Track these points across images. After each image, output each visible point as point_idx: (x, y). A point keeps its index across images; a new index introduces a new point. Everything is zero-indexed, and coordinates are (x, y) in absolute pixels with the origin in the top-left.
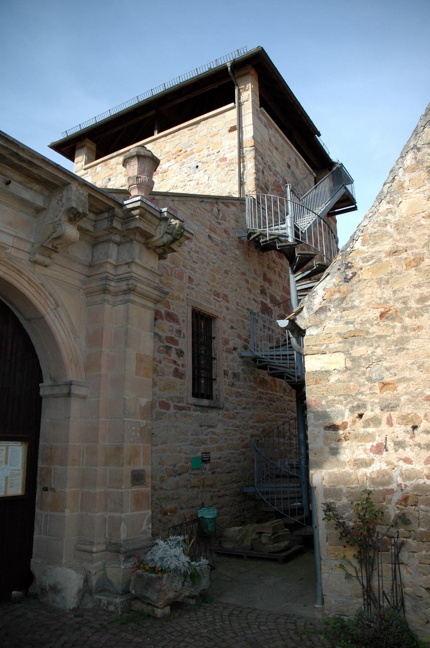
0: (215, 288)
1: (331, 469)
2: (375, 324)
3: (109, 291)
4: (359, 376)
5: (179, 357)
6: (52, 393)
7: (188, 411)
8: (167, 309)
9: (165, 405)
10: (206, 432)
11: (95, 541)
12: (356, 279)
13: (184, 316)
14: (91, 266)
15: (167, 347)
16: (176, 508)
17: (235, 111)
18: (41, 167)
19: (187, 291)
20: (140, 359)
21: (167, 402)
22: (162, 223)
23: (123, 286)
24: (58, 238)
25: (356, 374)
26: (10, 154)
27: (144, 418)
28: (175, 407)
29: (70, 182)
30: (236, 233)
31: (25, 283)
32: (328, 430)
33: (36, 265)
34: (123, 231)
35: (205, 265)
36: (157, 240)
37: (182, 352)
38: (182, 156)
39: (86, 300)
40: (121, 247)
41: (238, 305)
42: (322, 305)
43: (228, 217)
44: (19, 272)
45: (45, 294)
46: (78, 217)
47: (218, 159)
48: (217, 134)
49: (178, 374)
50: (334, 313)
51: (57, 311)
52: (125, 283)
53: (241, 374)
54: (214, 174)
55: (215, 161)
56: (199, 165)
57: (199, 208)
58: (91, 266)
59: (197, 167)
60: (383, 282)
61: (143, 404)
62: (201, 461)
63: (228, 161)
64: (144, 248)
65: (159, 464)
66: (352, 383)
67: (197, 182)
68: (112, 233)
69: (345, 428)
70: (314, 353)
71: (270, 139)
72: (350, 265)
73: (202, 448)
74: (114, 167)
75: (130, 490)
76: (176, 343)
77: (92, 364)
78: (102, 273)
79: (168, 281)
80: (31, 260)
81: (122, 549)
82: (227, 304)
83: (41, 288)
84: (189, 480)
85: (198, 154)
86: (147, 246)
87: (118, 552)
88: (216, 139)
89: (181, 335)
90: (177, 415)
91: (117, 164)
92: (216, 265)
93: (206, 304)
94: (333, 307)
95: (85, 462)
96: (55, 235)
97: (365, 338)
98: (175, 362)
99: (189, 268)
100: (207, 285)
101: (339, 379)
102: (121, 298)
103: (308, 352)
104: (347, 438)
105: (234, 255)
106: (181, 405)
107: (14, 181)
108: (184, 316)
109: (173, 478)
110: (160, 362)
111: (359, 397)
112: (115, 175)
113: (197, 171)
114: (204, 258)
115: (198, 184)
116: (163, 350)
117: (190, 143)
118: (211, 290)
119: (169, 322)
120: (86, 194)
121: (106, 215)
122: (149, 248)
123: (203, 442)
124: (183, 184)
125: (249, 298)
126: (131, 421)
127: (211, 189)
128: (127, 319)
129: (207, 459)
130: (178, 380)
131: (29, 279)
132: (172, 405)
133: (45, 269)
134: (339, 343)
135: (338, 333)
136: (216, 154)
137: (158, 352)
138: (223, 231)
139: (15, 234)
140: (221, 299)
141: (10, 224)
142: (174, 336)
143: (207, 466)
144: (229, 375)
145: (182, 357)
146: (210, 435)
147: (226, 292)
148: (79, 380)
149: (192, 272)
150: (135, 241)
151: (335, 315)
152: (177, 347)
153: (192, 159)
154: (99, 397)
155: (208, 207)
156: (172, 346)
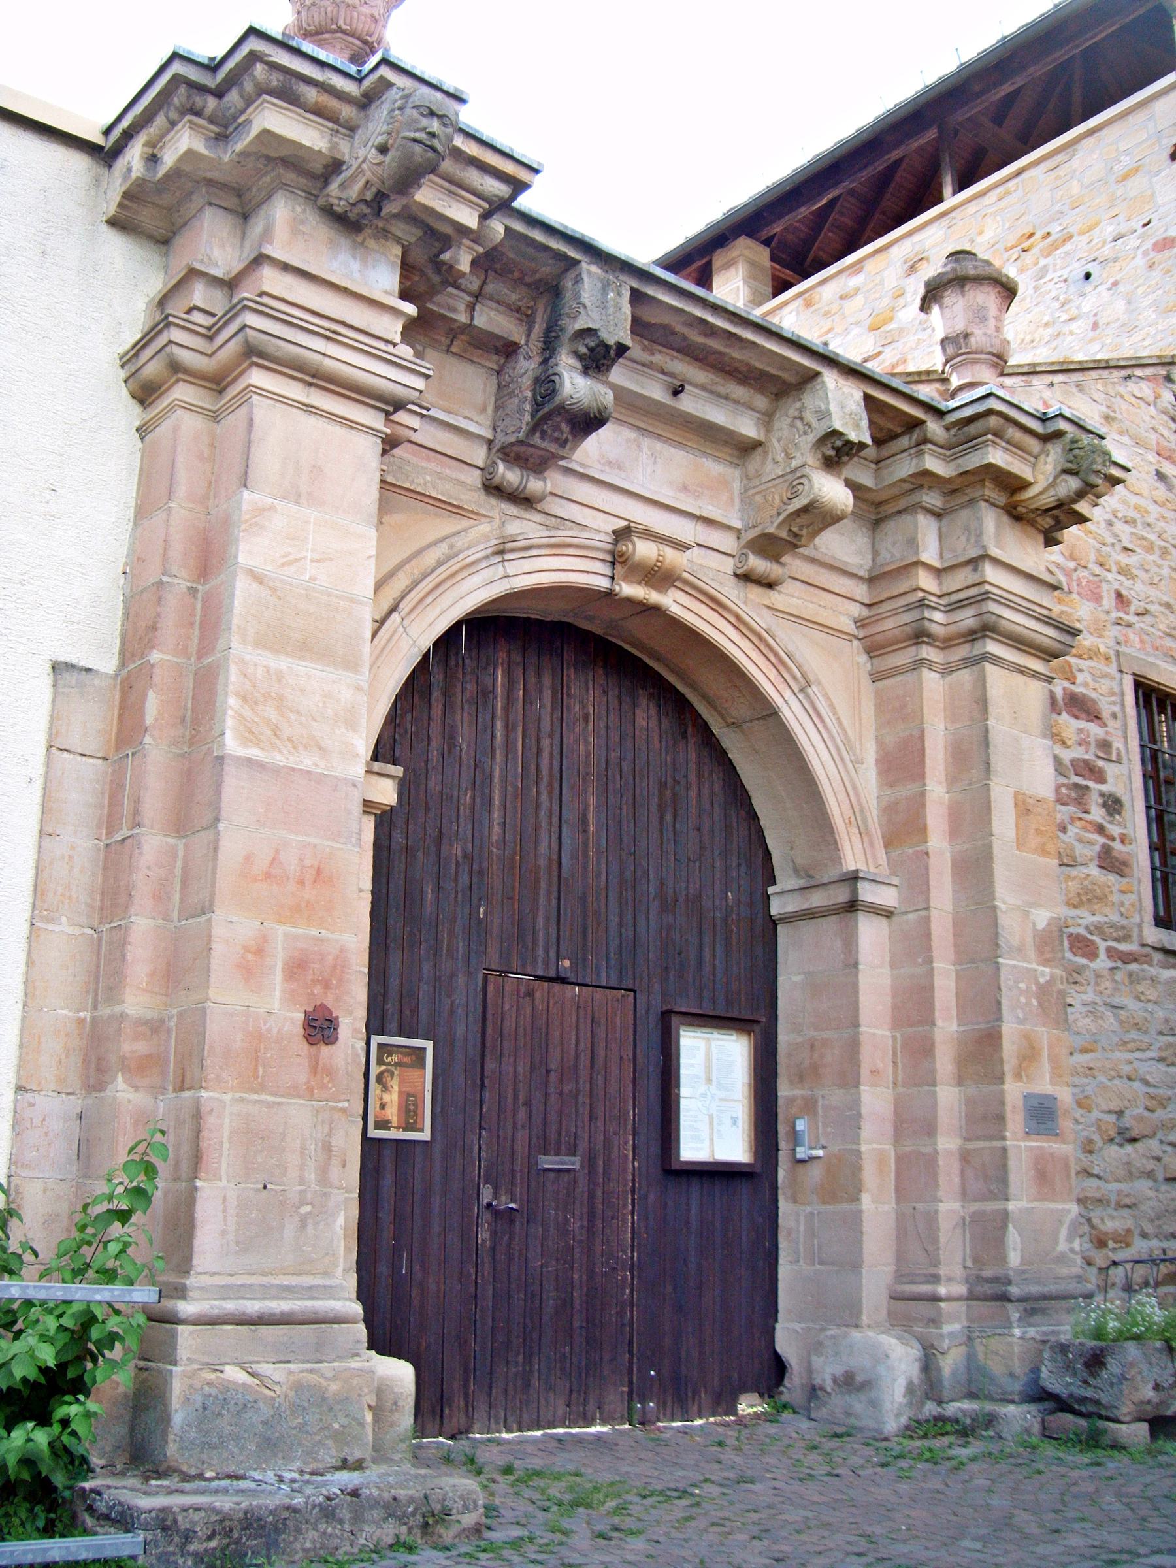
3: (929, 635)
5: (1111, 815)
6: (805, 906)
7: (1145, 966)
8: (1066, 684)
9: (1083, 946)
11: (942, 1272)
13: (1114, 703)
14: (872, 580)
15: (1076, 786)
16: (1129, 1231)
18: (753, 343)
19: (1114, 632)
20: (1024, 807)
22: (1049, 446)
23: (967, 619)
24: (805, 510)
26: (684, 324)
27: (1046, 962)
28: (1111, 952)
29: (819, 369)
33: (749, 585)
34: (948, 481)
35: (1155, 557)
36: (1041, 493)
38: (1035, 251)
39: (869, 666)
40: (945, 521)
44: (716, 604)
45: (776, 655)
46: (847, 455)
47: (1148, 245)
48: (1137, 170)
49: (1110, 862)
51: (808, 696)
52: (970, 612)
54: (1140, 290)
55: (1140, 252)
56: (1090, 268)
57: (1122, 396)
58: (872, 580)
59: (1088, 276)
61: (1041, 925)
64: (1006, 519)
65: (1079, 1104)
67: (1092, 320)
68: (921, 486)
74: (835, 307)
75: (1022, 1144)
76: (1100, 778)
77: (904, 827)
78: (906, 593)
79: (1065, 609)
80: (739, 572)
81: (1014, 1290)
84: (1159, 1159)
85: (1085, 238)
86: (1016, 515)
87: (1004, 1298)
88: (1136, 185)
89: (1109, 753)
91: (841, 298)
95: (900, 1078)
96: (797, 504)
99: (1114, 569)
100: (1167, 612)
102: (963, 651)
106: (1123, 947)
107: (690, 383)
108: (1114, 703)
109: (1116, 1148)
112: (838, 329)
113: (1088, 287)
114: (1153, 537)
115: (1095, 326)
116: (1069, 796)
117: (1057, 208)
119: (1077, 718)
120: (858, 395)
121: (905, 441)
122: (1017, 518)
124: (1049, 331)
126: (1014, 966)
127: (1137, 337)
128: (982, 703)
130: (1112, 878)
131: (738, 617)
132: (1102, 946)
133: (771, 593)
136: (1140, 231)
139: (698, 513)
141: (685, 489)
145: (1120, 814)
148: (872, 870)
150: (983, 504)
152: (1104, 788)
153: (1067, 254)
154: (927, 909)
156: (1091, 784)
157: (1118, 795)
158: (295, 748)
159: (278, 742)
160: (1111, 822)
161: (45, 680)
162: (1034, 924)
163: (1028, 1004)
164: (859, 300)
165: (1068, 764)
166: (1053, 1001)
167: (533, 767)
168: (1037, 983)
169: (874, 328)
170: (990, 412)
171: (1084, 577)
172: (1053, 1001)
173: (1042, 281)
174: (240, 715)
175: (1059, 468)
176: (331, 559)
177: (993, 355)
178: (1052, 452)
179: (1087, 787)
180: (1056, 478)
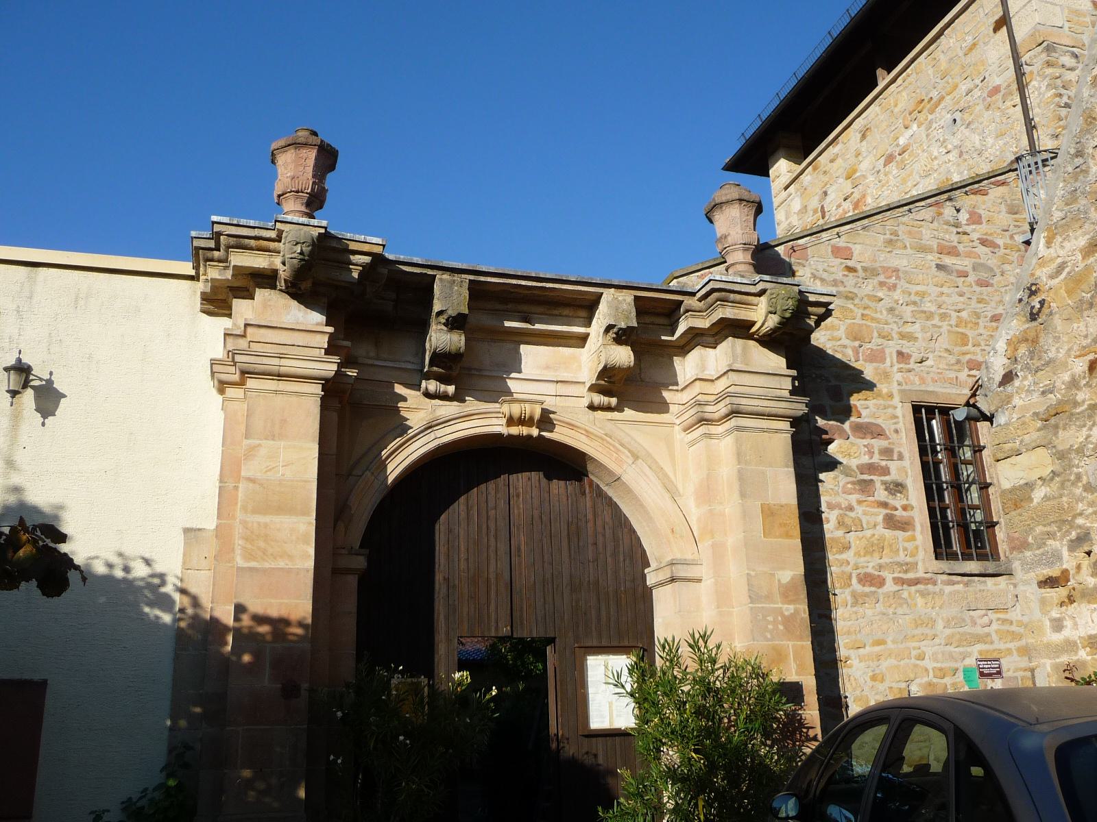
0: (968, 357)
2: (1084, 385)
4: (1073, 484)
12: (1045, 310)
18: (553, 288)
25: (1069, 480)
27: (790, 602)
30: (1016, 237)
31: (583, 438)
38: (925, 111)
45: (614, 446)
50: (1023, 381)
56: (958, 116)
60: (1085, 306)
62: (977, 674)
63: (1003, 92)
66: (1065, 499)
69: (1068, 581)
70: (1006, 455)
72: (1034, 288)
73: (976, 650)
76: (886, 471)
83: (606, 440)
90: (905, 595)
92: (964, 314)
94: (1021, 370)
97: (1072, 414)
100: (946, 355)
104: (1072, 598)
106: (911, 575)
111: (1080, 521)
118: (958, 362)
119: (863, 438)
123: (980, 639)
126: (763, 607)
132: (889, 577)
135: (1034, 413)
136: (980, 84)
142: (877, 461)
146: (995, 626)
151: (1026, 383)
152: (887, 478)
155: (927, 214)
158: (275, 558)
159: (265, 557)
161: (180, 538)
162: (779, 581)
164: (839, 161)
165: (855, 468)
167: (484, 526)
169: (848, 178)
170: (713, 291)
173: (931, 130)
174: (245, 548)
176: (292, 464)
177: (745, 244)
179: (872, 480)
180: (766, 317)
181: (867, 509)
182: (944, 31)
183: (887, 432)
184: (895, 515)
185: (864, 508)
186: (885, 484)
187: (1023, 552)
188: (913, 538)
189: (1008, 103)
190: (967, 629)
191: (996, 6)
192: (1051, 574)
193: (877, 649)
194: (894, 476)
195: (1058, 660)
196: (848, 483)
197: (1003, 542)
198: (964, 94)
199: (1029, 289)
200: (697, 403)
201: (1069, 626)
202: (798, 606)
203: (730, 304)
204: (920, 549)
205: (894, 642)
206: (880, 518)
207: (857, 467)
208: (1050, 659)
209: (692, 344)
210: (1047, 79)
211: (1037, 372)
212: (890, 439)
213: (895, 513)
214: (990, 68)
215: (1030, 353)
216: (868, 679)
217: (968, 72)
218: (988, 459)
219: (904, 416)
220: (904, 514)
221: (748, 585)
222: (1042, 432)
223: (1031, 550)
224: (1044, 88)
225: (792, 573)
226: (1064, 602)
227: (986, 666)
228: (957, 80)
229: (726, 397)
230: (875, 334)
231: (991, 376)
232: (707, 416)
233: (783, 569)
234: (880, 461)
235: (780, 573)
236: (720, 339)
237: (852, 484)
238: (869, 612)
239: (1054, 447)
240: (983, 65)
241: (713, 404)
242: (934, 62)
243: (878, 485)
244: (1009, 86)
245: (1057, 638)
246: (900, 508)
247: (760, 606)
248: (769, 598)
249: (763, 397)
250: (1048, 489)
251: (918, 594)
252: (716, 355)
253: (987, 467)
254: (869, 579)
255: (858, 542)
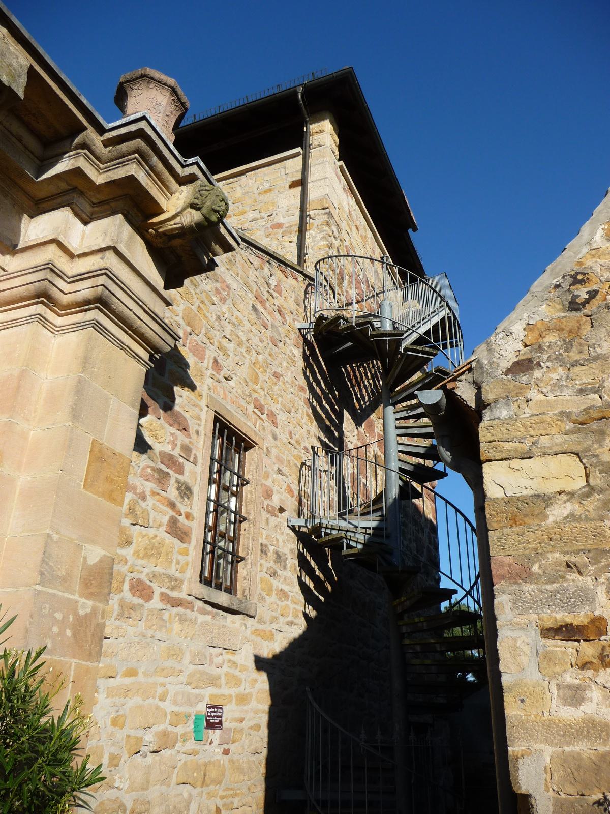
1: (568, 745)
5: (182, 497)
7: (188, 611)
10: (219, 660)
17: (300, 158)
21: (148, 583)
27: (90, 596)
28: (165, 598)
32: (553, 639)
37: (188, 489)
41: (291, 437)
42: (521, 357)
43: (284, 292)
49: (177, 531)
50: (549, 373)
53: (289, 557)
61: (93, 560)
70: (505, 456)
71: (349, 211)
72: (580, 277)
73: (208, 694)
76: (180, 470)
82: (274, 428)
89: (190, 456)
90: (166, 615)
92: (260, 357)
93: (239, 416)
94: (548, 360)
98: (172, 505)
101: (572, 515)
103: (491, 456)
105: (290, 354)
106: (175, 594)
110: (144, 498)
118: (250, 395)
119: (171, 425)
123: (214, 681)
125: (308, 431)
126: (54, 595)
129: (217, 720)
130: (176, 542)
132: (157, 591)
134: (568, 433)
136: (266, 218)
137: (142, 476)
138: (276, 308)
140: (264, 417)
142: (177, 455)
143: (215, 735)
144: (269, 554)
145: (188, 498)
146: (225, 669)
147: (275, 407)
149: (221, 353)
151: (554, 376)
152: (180, 477)
157: (190, 485)
160: (181, 503)
162: (85, 558)
163: (62, 633)
165: (158, 454)
166: (89, 634)
168: (76, 614)
171: (195, 341)
172: (89, 634)
175: (188, 202)
178: (185, 192)
179: (168, 474)
180: (184, 209)
181: (158, 504)
182: (248, 172)
183: (191, 429)
184: (179, 521)
185: (155, 502)
186: (179, 483)
187: (519, 584)
188: (185, 553)
189: (286, 238)
190: (206, 668)
191: (297, 172)
192: (569, 620)
193: (128, 680)
194: (185, 478)
195: (567, 749)
196: (149, 467)
197: (245, 579)
198: (250, 220)
199: (574, 277)
200: (50, 266)
201: (595, 700)
202: (98, 604)
203: (147, 168)
204: (190, 567)
205: (146, 674)
206: (166, 519)
207: (160, 453)
208: (551, 744)
209: (59, 201)
210: (324, 233)
211: (573, 366)
212: (191, 438)
213: (179, 518)
214: (278, 210)
215: (564, 344)
216: (109, 723)
217: (259, 206)
218: (249, 496)
219: (206, 421)
220: (186, 522)
221: (44, 553)
222: (573, 437)
223: (536, 583)
224: (319, 238)
225: (104, 552)
226: (591, 663)
227: (213, 714)
228: (247, 208)
229: (100, 275)
230: (203, 331)
231: (494, 360)
232: (54, 292)
233: (93, 542)
234: (179, 457)
235: (89, 547)
236: (101, 212)
237: (151, 470)
238: (131, 631)
239: (596, 456)
240: (273, 206)
241: (69, 280)
242: (231, 190)
243: (172, 481)
244: (291, 227)
245: (569, 714)
246: (184, 515)
247: (51, 591)
248: (65, 581)
249: (141, 303)
250: (577, 507)
251: (177, 619)
252: (84, 231)
253: (246, 502)
254: (140, 588)
255: (140, 540)
